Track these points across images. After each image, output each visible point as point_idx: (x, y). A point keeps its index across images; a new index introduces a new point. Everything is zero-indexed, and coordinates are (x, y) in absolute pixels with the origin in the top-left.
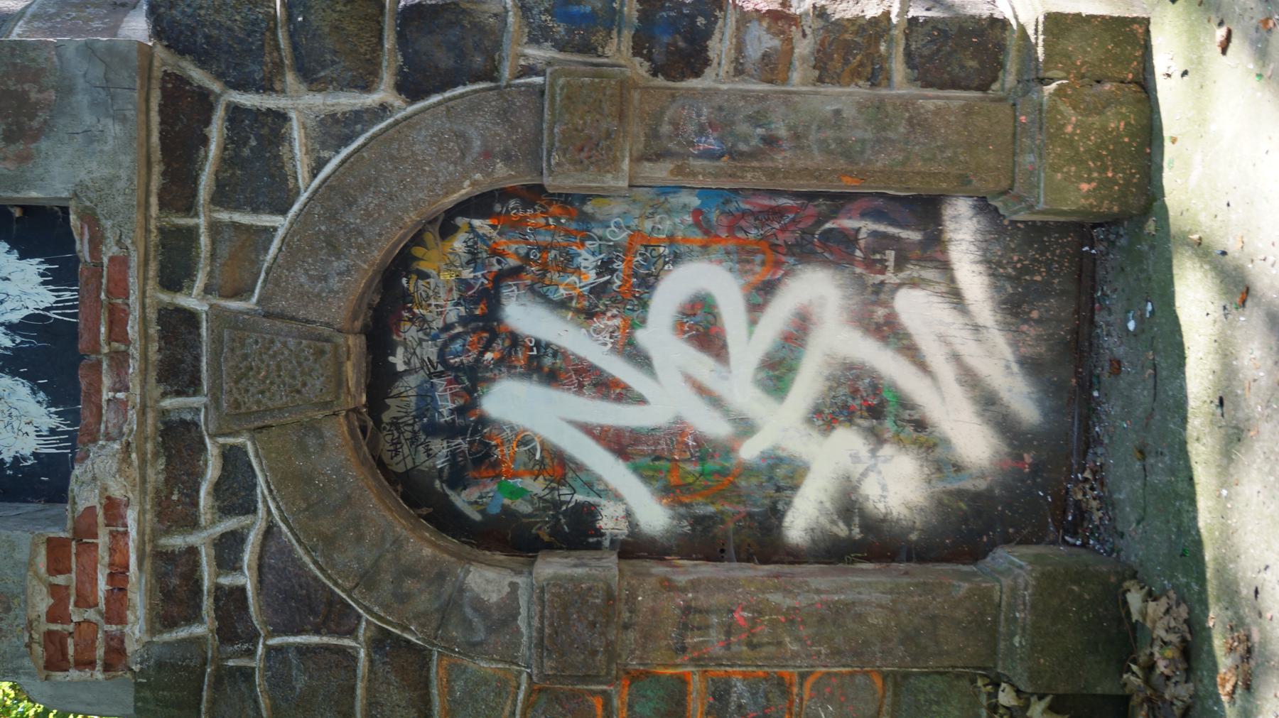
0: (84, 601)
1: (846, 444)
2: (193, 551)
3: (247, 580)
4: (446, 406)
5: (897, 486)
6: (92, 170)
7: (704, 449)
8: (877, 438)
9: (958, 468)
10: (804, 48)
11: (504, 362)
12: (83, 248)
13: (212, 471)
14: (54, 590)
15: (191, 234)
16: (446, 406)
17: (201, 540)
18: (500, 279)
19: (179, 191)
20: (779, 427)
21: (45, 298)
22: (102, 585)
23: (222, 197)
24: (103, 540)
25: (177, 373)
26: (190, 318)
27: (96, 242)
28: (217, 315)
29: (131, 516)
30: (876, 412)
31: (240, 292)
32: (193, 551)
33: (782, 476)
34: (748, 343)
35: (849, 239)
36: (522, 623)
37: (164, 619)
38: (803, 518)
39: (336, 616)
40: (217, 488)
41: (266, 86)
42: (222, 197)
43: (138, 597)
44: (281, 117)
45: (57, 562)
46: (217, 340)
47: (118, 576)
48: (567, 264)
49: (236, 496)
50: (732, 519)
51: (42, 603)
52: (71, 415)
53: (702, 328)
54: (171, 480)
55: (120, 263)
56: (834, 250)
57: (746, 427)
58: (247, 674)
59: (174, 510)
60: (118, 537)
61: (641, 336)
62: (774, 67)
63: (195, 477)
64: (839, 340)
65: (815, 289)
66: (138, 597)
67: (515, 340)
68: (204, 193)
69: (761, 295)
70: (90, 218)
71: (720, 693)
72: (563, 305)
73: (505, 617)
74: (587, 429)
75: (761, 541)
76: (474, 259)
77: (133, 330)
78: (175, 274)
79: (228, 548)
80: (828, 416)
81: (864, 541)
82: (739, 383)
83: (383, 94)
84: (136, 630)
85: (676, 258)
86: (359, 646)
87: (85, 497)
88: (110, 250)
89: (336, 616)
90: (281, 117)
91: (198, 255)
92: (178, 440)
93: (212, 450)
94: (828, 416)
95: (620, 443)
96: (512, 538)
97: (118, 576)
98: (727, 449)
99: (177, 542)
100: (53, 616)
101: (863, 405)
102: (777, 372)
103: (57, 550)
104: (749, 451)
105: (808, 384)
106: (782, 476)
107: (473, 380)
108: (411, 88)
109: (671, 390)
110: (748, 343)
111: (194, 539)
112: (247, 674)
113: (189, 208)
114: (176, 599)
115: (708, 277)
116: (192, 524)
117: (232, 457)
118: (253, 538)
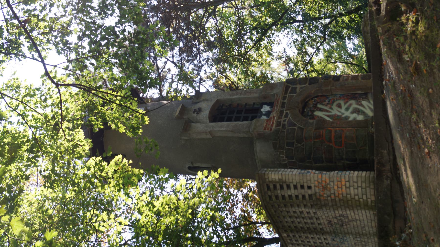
0: (269, 125)
1: (355, 115)
3: (286, 123)
4: (310, 113)
5: (360, 118)
7: (338, 116)
8: (358, 114)
9: (369, 116)
10: (350, 78)
11: (317, 110)
13: (284, 114)
15: (286, 96)
16: (310, 113)
17: (282, 120)
18: (317, 103)
21: (270, 109)
22: (271, 123)
24: (272, 120)
29: (275, 118)
30: (359, 112)
33: (349, 117)
35: (356, 97)
36: (314, 124)
37: (276, 126)
39: (295, 125)
40: (285, 116)
41: (296, 85)
43: (274, 125)
44: (297, 87)
48: (325, 101)
49: (286, 116)
51: (265, 125)
55: (279, 98)
57: (343, 114)
58: (284, 132)
59: (280, 117)
61: (332, 107)
62: (347, 80)
66: (274, 125)
67: (318, 108)
69: (345, 103)
71: (336, 131)
72: (323, 105)
73: (313, 123)
74: (325, 115)
76: (315, 101)
79: (284, 121)
80: (352, 113)
82: (343, 110)
83: (307, 85)
84: (274, 127)
85: (337, 100)
86: (296, 128)
87: (271, 116)
89: (295, 125)
90: (297, 87)
92: (282, 112)
95: (328, 116)
98: (341, 116)
100: (266, 126)
102: (347, 109)
104: (343, 116)
105: (351, 110)
107: (314, 111)
108: (309, 84)
109: (335, 111)
112: (284, 132)
113: (281, 118)
114: (278, 124)
117: (287, 113)
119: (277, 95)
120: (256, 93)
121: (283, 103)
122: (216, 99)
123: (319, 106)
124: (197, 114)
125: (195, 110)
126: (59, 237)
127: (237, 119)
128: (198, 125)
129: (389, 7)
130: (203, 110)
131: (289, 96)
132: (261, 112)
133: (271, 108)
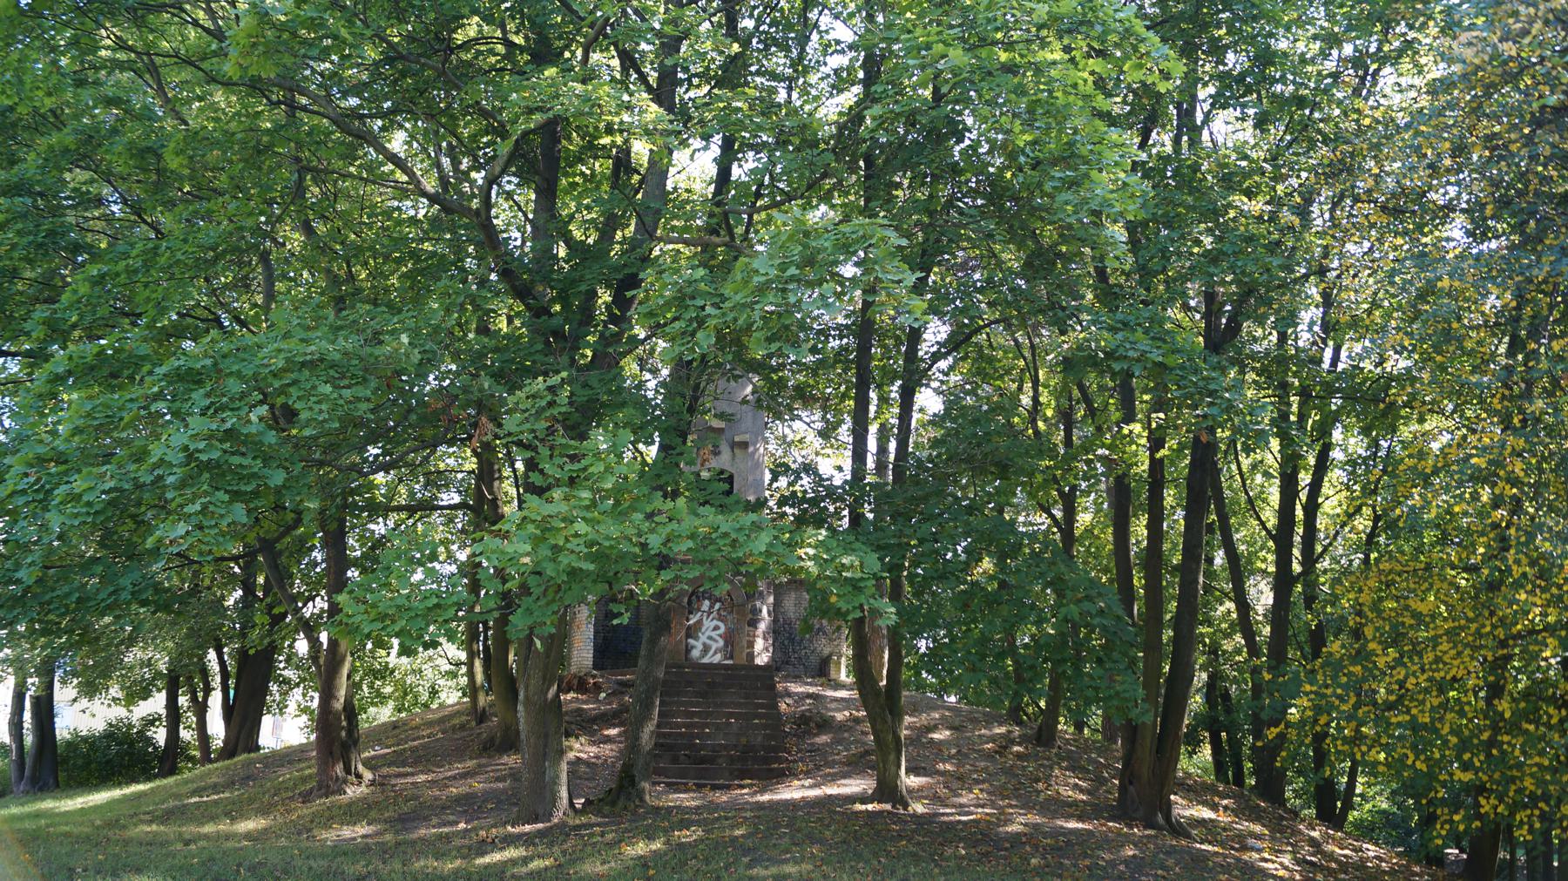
20: (703, 638)
22: (872, 444)
33: (697, 638)
34: (714, 634)
38: (691, 641)
50: (692, 632)
53: (716, 628)
56: (726, 645)
64: (714, 646)
65: (721, 643)
75: (688, 636)
80: (704, 644)
81: (688, 649)
91: (60, 799)
94: (704, 644)
96: (690, 602)
101: (706, 649)
102: (710, 638)
106: (697, 638)
109: (708, 624)
110: (714, 634)
115: (722, 630)
123: (717, 606)
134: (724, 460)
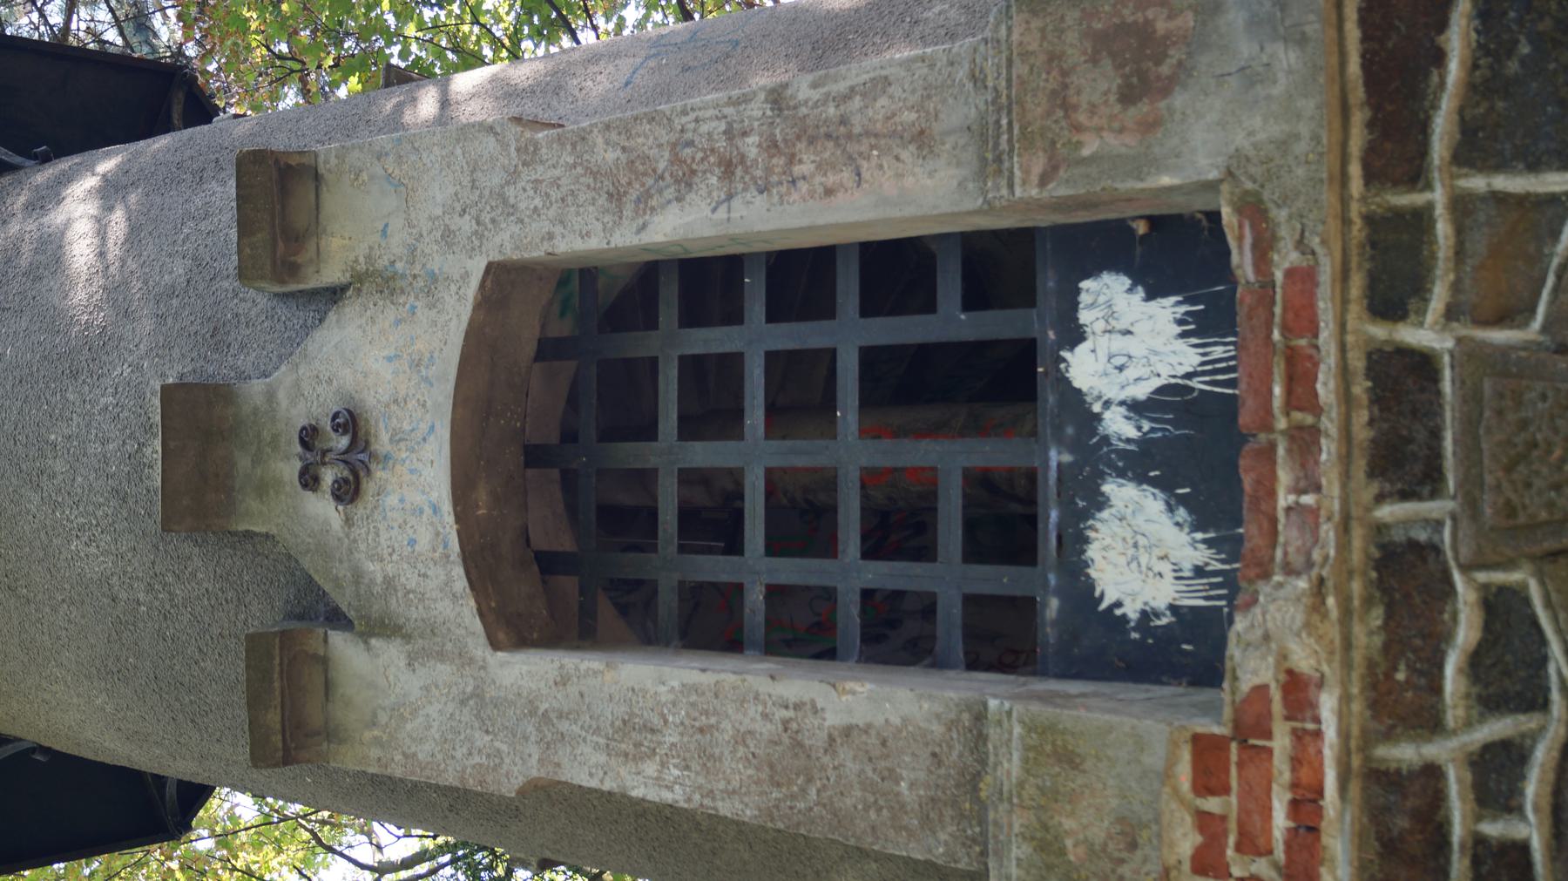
2: (1432, 772)
3: (1532, 830)
6: (1255, 129)
12: (1242, 261)
13: (1466, 631)
14: (1204, 821)
15: (1421, 220)
17: (1448, 752)
19: (1396, 150)
22: (1280, 820)
23: (1470, 152)
24: (1281, 742)
25: (1402, 461)
26: (1423, 364)
27: (1263, 250)
28: (1469, 353)
29: (1328, 704)
31: (1502, 318)
32: (1432, 772)
40: (1476, 664)
42: (1470, 152)
45: (1209, 780)
46: (1471, 397)
47: (1306, 804)
51: (1186, 841)
52: (1228, 545)
54: (1393, 647)
55: (1303, 278)
59: (1401, 701)
60: (1306, 739)
63: (1437, 641)
68: (1440, 145)
70: (1254, 209)
77: (1326, 388)
78: (1393, 295)
79: (1497, 771)
87: (1251, 669)
88: (1286, 258)
92: (1405, 579)
93: (1465, 591)
97: (1306, 804)
99: (1405, 753)
103: (1207, 751)
111: (1434, 750)
113: (1416, 177)
116: (1430, 723)
117: (1502, 609)
118: (1543, 755)
119: (1254, 209)
120: (922, 140)
121: (1401, 379)
122: (477, 267)
124: (339, 496)
125: (309, 437)
126: (449, 646)
127: (803, 633)
128: (391, 653)
129: (536, 18)
130: (382, 442)
131: (1461, 206)
132: (1076, 405)
133: (1200, 327)
134: (399, 365)
